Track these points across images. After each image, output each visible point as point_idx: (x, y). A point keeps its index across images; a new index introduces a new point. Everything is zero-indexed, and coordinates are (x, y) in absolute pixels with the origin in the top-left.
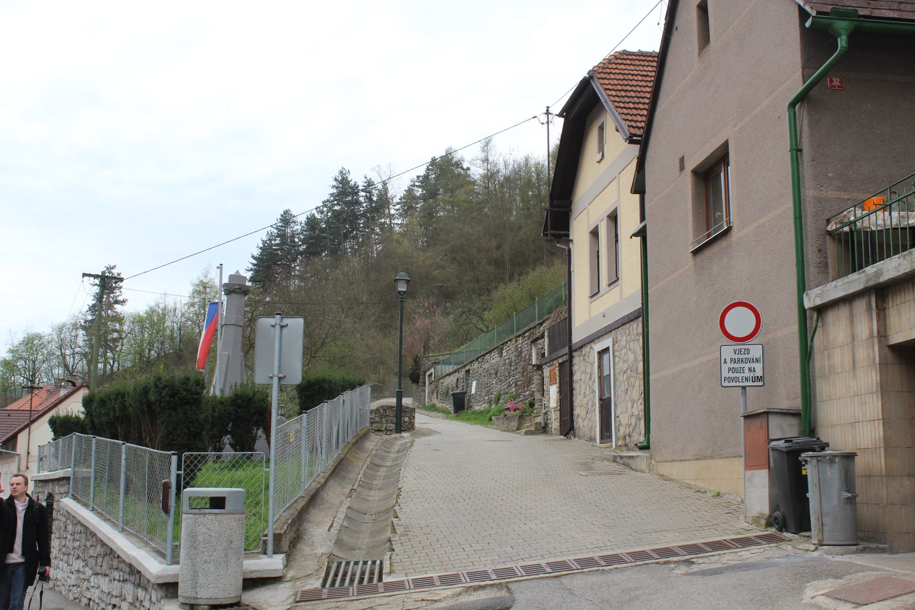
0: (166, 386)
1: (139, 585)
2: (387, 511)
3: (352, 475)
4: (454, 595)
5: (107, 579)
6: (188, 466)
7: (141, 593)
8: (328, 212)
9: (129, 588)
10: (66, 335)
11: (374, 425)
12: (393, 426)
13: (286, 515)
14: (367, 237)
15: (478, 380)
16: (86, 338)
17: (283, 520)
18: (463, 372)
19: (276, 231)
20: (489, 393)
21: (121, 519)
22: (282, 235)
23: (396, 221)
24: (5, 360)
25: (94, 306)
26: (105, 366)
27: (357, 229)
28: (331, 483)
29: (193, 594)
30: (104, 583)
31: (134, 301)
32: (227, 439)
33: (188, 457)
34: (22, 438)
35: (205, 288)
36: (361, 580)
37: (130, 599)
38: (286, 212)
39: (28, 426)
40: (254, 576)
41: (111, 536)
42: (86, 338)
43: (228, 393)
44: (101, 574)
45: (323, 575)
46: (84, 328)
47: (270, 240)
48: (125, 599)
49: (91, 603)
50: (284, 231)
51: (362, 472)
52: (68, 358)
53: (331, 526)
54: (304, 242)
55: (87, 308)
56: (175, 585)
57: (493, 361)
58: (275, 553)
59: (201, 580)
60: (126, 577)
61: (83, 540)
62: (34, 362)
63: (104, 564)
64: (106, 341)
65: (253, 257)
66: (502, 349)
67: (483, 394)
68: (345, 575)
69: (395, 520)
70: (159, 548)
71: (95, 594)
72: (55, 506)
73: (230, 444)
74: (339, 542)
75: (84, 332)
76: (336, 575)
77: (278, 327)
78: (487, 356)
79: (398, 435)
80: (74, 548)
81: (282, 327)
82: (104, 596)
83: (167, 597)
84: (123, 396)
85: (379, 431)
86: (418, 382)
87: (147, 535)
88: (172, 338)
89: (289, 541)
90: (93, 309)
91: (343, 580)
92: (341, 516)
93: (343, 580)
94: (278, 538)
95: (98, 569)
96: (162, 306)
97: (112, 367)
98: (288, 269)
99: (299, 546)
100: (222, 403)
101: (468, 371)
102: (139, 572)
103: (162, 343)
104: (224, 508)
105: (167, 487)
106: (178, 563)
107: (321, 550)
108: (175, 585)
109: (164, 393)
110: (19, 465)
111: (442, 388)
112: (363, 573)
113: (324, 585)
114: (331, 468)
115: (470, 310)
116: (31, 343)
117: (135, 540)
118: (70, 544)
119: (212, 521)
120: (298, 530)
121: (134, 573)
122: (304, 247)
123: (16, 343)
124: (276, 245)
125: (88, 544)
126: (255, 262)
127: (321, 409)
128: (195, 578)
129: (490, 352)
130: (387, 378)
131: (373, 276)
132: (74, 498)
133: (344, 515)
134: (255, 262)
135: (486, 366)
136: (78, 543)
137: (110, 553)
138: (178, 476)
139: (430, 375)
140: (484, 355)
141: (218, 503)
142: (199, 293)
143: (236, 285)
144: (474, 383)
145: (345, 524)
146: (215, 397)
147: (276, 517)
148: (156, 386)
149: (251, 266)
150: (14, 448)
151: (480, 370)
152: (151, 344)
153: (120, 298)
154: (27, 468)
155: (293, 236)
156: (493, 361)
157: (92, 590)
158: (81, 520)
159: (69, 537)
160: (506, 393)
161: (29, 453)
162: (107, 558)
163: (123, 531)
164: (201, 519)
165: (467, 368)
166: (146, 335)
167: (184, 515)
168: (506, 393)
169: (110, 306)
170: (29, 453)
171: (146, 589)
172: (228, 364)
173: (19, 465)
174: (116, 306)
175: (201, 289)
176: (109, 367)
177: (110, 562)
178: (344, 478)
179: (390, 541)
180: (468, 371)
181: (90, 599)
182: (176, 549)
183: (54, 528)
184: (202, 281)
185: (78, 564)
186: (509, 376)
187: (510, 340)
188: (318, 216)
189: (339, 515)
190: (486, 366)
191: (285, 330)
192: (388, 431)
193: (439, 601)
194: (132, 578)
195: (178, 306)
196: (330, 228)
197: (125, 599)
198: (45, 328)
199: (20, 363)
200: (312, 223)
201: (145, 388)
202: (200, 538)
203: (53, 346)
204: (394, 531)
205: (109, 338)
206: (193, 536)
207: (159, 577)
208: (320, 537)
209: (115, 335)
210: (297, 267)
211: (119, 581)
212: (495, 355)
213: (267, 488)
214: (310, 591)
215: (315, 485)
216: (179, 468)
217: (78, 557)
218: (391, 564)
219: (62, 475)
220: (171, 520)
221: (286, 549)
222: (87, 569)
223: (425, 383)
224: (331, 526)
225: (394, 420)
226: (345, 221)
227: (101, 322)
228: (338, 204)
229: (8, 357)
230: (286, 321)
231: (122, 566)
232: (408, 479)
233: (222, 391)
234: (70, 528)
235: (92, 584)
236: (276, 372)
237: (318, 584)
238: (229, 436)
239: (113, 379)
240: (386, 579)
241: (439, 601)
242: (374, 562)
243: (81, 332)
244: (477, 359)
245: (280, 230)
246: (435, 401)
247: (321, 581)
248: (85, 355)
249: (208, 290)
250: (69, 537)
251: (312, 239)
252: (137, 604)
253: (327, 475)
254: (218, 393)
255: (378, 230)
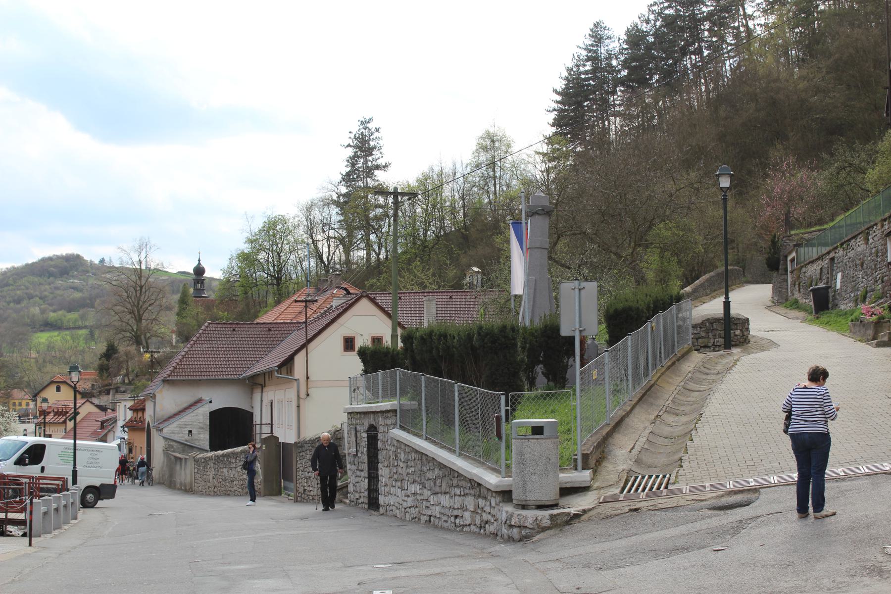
0: (487, 334)
1: (479, 496)
2: (686, 434)
3: (661, 402)
4: (717, 497)
5: (448, 496)
6: (513, 403)
7: (481, 502)
8: (656, 20)
9: (470, 502)
10: (317, 215)
11: (700, 340)
12: (721, 341)
13: (594, 438)
14: (716, 49)
15: (843, 272)
16: (341, 218)
17: (590, 443)
18: (826, 262)
19: (585, 53)
20: (855, 289)
21: (457, 446)
22: (594, 58)
23: (757, 21)
24: (243, 253)
25: (348, 174)
26: (368, 255)
27: (701, 40)
28: (637, 410)
29: (524, 498)
30: (445, 500)
31: (399, 170)
32: (539, 369)
33: (513, 396)
34: (299, 359)
35: (493, 141)
36: (652, 488)
37: (471, 508)
38: (597, 25)
39: (304, 346)
40: (568, 486)
41: (452, 460)
42: (341, 218)
43: (538, 324)
44: (441, 493)
45: (622, 485)
46: (337, 203)
47: (577, 66)
48: (467, 510)
49: (432, 519)
50: (595, 52)
51: (671, 398)
52: (320, 245)
53: (633, 448)
54: (625, 64)
55: (339, 178)
56: (510, 492)
57: (859, 249)
58: (584, 468)
59: (529, 487)
60: (467, 491)
61: (419, 466)
62: (279, 254)
63: (444, 485)
64: (367, 219)
65: (555, 91)
66: (868, 234)
67: (849, 289)
68: (639, 485)
69: (689, 443)
70: (494, 466)
71: (436, 511)
72: (380, 436)
73: (543, 373)
74: (638, 462)
75: (337, 210)
76: (632, 485)
77: (577, 290)
78: (853, 242)
79: (728, 351)
80: (408, 474)
81: (580, 290)
82: (446, 511)
83: (503, 501)
84: (445, 336)
85: (706, 347)
86: (777, 269)
87: (486, 458)
88: (453, 210)
89: (595, 459)
90: (347, 178)
91: (637, 490)
92: (643, 440)
93: (637, 490)
94: (585, 457)
95: (437, 489)
96: (437, 169)
97: (378, 255)
98: (604, 107)
99: (604, 464)
100: (532, 334)
101: (832, 259)
102: (479, 485)
103: (442, 219)
104: (542, 434)
105: (499, 419)
106: (511, 476)
107: (621, 467)
108: (510, 492)
109: (486, 340)
110: (298, 392)
111: (805, 280)
112: (653, 484)
113: (622, 492)
114: (639, 396)
115: (851, 165)
116: (274, 230)
117: (472, 461)
118: (403, 471)
119: (537, 446)
120: (603, 452)
121: (476, 486)
122: (625, 73)
123: (256, 230)
124: (586, 73)
125: (425, 469)
126: (559, 98)
127: (625, 344)
128: (524, 486)
129: (855, 237)
130: (748, 256)
131: (722, 113)
132: (402, 428)
133: (645, 439)
134: (559, 98)
135: (851, 254)
136: (412, 469)
137: (450, 473)
138: (507, 411)
139: (792, 260)
140: (849, 240)
141: (538, 430)
142: (485, 149)
143: (539, 206)
144: (839, 275)
145: (646, 446)
146: (525, 328)
147: (583, 443)
148: (479, 334)
149: (556, 106)
150: (290, 371)
151: (846, 259)
152: (427, 224)
153: (382, 162)
154: (308, 395)
155: (609, 57)
156: (859, 249)
157: (433, 508)
158: (417, 448)
159: (401, 464)
160: (873, 290)
161: (308, 378)
162: (445, 480)
163: (460, 455)
164: (527, 443)
165: (832, 255)
166: (419, 210)
167: (514, 441)
168: (873, 290)
169: (369, 172)
170: (308, 378)
171: (485, 498)
172: (535, 289)
173: (298, 392)
174: (376, 172)
175: (488, 142)
176: (373, 254)
177: (450, 482)
178: (652, 404)
179: (681, 459)
180: (832, 259)
181: (430, 516)
182: (508, 467)
183: (380, 457)
184: (488, 133)
185: (415, 488)
186: (875, 269)
187: (876, 224)
188: (644, 27)
189: (641, 439)
190: (851, 254)
191: (583, 292)
192: (715, 347)
193: (705, 500)
194: (473, 492)
195: (459, 169)
196: (661, 43)
197: (467, 510)
198: (289, 205)
199: (262, 256)
200: (635, 38)
201: (469, 334)
202: (527, 456)
203: (301, 233)
204: (686, 451)
205: (371, 215)
206: (521, 455)
207: (497, 486)
208: (622, 456)
209: (379, 211)
210: (618, 98)
211: (460, 495)
212: (860, 240)
213: (575, 418)
214: (611, 496)
215: (621, 413)
216: (507, 405)
217: (414, 481)
218: (677, 477)
219: (389, 408)
220: (503, 445)
221: (593, 465)
222: (425, 490)
223: (786, 270)
224: (633, 448)
225: (722, 333)
226: (682, 29)
227: (360, 199)
228: (669, 7)
229: (247, 248)
230: (584, 284)
231: (463, 483)
232: (715, 406)
233: (531, 321)
234: (402, 456)
235: (432, 502)
236: (577, 326)
237: (617, 491)
238: (541, 366)
239: (380, 273)
240: (670, 487)
241: (705, 500)
242: (664, 476)
243: (334, 210)
244: (842, 244)
245: (590, 51)
246: (797, 295)
247: (619, 489)
248: (342, 241)
249: (497, 144)
250: (401, 464)
251: (634, 60)
252: (479, 511)
253: (633, 403)
254: (527, 323)
255: (730, 39)
